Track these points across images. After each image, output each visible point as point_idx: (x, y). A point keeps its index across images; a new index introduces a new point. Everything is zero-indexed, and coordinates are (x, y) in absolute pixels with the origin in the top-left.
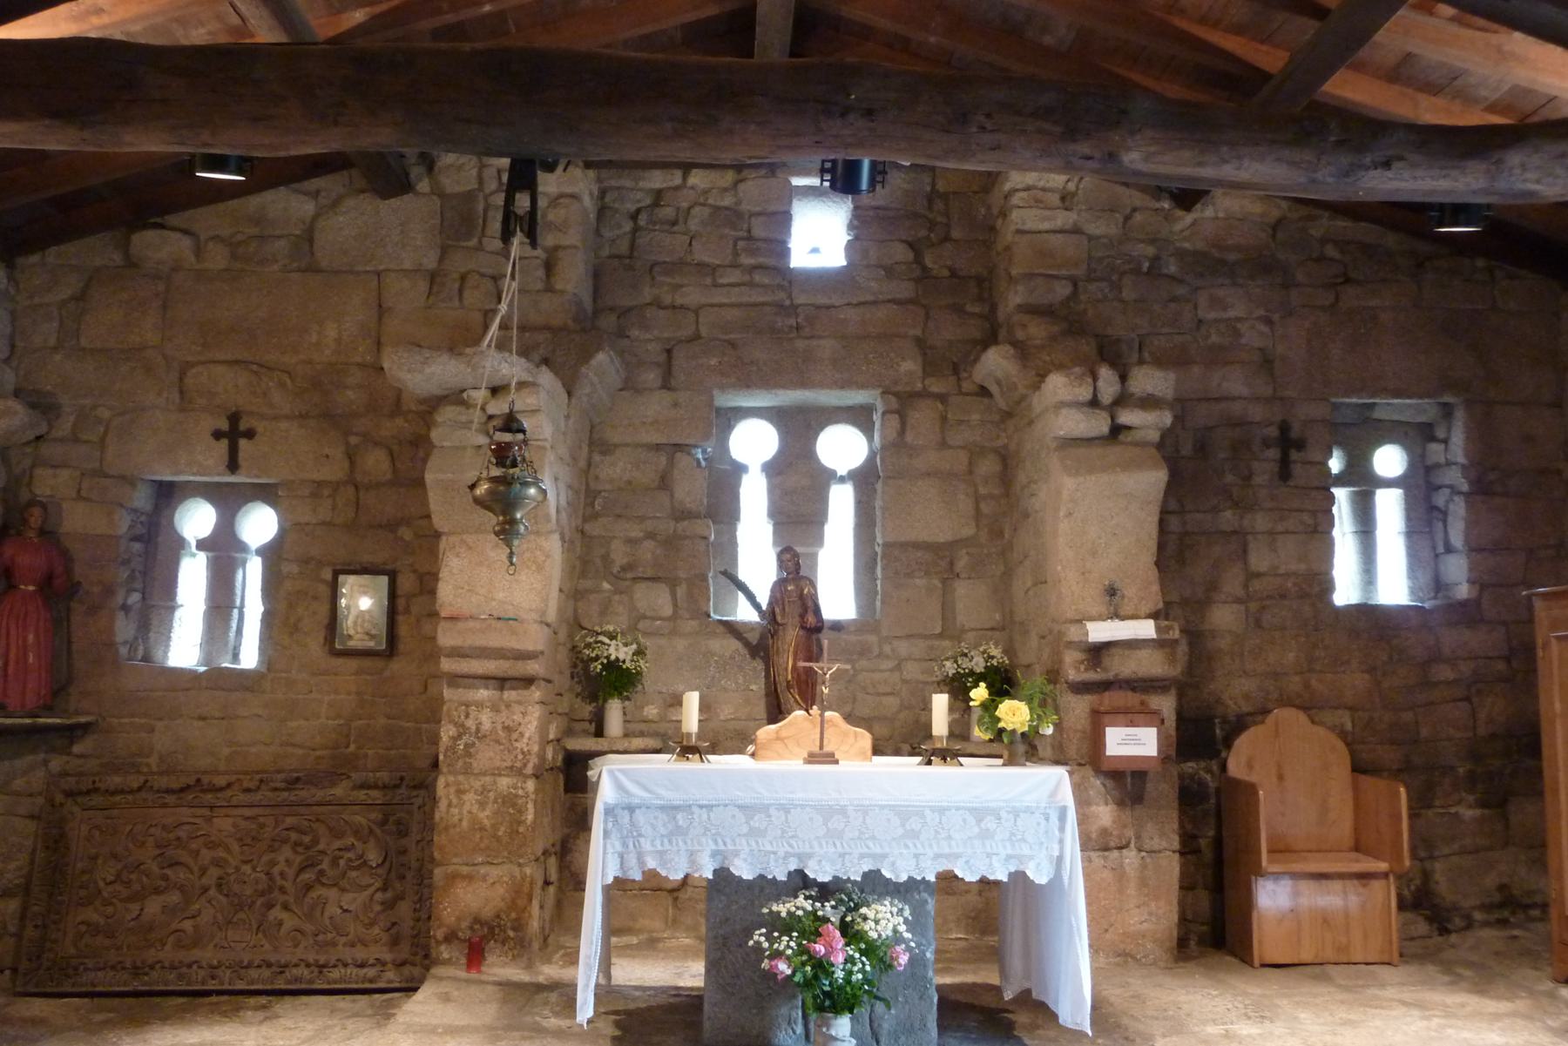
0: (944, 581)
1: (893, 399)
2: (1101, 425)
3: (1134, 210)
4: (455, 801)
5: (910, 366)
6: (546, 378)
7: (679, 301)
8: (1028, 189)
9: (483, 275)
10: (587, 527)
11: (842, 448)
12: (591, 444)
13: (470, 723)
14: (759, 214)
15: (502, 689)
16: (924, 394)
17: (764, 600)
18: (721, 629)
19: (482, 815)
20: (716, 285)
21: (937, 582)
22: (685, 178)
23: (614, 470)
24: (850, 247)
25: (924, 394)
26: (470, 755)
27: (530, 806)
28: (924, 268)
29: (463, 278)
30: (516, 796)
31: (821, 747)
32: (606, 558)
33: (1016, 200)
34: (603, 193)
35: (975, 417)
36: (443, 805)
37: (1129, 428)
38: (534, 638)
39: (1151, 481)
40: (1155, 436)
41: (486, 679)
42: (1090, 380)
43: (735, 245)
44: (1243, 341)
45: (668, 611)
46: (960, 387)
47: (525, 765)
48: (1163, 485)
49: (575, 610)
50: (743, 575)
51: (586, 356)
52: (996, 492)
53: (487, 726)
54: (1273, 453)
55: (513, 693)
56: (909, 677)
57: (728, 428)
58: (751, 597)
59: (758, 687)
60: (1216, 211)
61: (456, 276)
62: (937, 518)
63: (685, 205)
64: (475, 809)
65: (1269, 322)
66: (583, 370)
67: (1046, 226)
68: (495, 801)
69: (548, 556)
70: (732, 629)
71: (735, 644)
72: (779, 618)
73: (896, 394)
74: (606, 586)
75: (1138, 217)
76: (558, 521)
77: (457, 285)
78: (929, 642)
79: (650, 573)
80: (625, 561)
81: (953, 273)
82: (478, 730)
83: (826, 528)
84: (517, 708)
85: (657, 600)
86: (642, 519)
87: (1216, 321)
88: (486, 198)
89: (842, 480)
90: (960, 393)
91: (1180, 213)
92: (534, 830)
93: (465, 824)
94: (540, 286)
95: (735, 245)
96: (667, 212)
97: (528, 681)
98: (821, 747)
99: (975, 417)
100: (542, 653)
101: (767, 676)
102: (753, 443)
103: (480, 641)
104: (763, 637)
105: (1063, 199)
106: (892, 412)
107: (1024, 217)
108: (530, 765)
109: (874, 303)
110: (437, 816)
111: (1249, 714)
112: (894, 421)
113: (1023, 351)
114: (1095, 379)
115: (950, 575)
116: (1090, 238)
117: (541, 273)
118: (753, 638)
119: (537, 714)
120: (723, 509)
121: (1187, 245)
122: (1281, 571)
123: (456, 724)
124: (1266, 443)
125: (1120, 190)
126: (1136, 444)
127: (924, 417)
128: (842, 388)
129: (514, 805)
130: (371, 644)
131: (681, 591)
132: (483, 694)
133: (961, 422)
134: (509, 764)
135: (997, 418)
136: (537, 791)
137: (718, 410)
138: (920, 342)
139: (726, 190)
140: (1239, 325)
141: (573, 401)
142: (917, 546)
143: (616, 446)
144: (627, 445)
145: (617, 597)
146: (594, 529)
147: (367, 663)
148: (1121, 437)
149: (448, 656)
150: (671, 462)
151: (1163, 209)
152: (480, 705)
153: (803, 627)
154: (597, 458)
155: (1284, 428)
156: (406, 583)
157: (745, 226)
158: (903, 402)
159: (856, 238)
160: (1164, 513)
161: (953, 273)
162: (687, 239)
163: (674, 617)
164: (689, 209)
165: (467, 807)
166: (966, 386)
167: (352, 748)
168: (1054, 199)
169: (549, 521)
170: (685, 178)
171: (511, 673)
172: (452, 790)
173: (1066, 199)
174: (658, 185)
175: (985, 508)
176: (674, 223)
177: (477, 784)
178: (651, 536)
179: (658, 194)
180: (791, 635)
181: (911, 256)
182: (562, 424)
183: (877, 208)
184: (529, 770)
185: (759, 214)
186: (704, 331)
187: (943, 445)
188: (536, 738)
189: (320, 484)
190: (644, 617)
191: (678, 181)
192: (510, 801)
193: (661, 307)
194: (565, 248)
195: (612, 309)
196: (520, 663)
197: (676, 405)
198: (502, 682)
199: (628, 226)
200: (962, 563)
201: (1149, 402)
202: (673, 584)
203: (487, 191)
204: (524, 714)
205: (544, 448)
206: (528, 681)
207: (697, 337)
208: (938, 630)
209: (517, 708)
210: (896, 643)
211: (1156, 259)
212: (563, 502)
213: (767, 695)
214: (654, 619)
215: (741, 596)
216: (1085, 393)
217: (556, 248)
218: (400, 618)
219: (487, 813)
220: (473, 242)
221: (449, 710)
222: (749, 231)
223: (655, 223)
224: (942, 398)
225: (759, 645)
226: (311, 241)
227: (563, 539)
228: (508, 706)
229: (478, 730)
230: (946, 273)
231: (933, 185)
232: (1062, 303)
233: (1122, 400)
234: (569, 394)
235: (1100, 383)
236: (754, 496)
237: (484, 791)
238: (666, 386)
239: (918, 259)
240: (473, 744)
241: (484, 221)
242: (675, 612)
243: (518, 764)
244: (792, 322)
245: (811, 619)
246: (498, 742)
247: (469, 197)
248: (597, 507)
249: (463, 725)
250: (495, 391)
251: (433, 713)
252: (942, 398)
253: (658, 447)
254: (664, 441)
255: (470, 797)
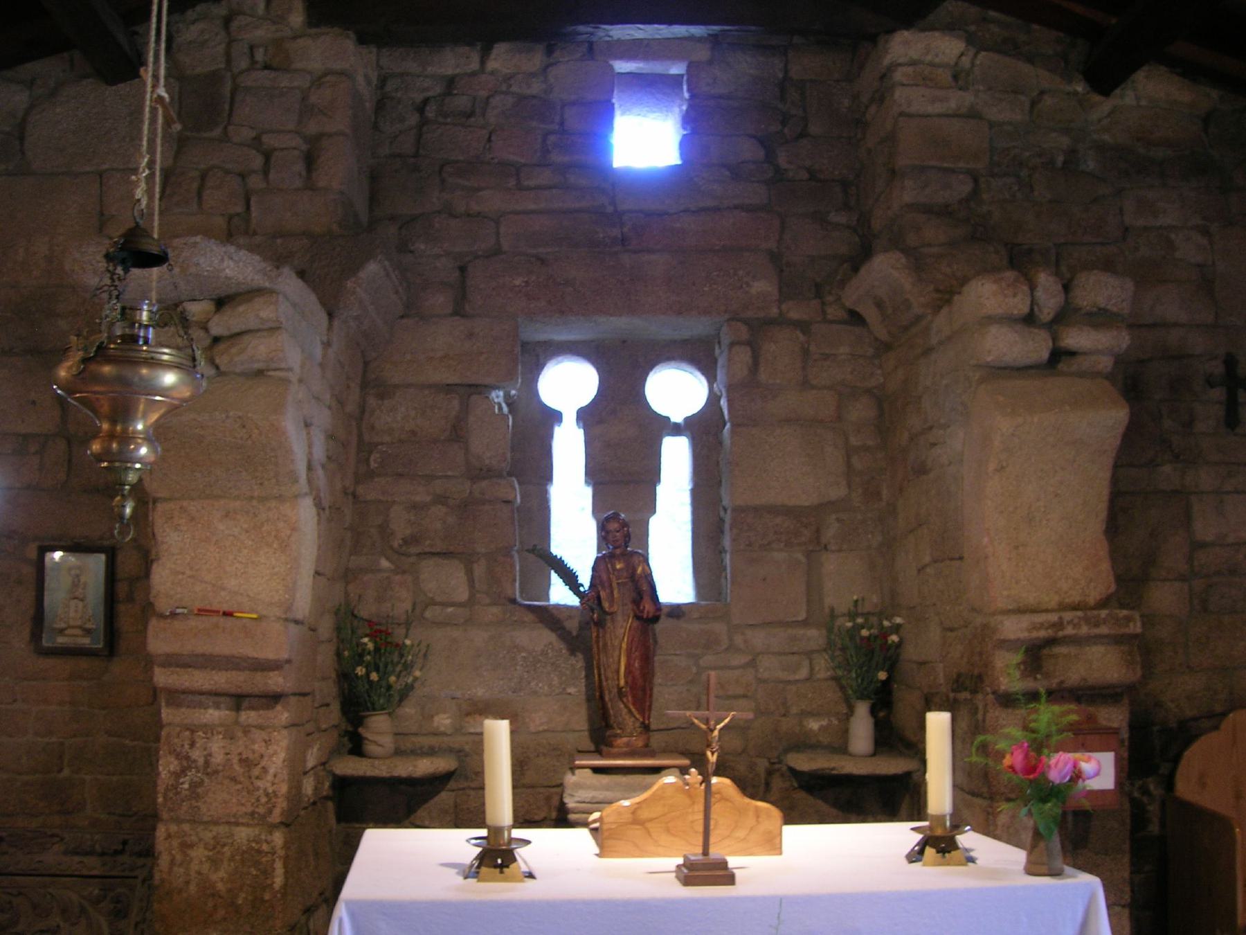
0: (808, 555)
1: (744, 329)
2: (1036, 347)
3: (1042, 93)
4: (179, 857)
5: (763, 286)
6: (289, 283)
7: (475, 208)
8: (913, 63)
9: (227, 172)
10: (360, 490)
11: (676, 391)
12: (364, 385)
13: (196, 754)
14: (573, 104)
15: (238, 708)
16: (781, 321)
17: (585, 579)
18: (529, 617)
19: (214, 877)
20: (520, 187)
21: (800, 557)
22: (483, 62)
23: (395, 417)
24: (684, 144)
25: (781, 321)
26: (197, 797)
27: (279, 865)
28: (777, 169)
29: (203, 177)
30: (259, 851)
31: (706, 852)
32: (385, 531)
33: (898, 76)
34: (383, 81)
35: (844, 350)
36: (164, 861)
37: (1072, 354)
38: (277, 643)
39: (1108, 420)
40: (1106, 363)
41: (216, 695)
42: (1026, 288)
43: (544, 140)
44: (1178, 255)
45: (463, 594)
46: (824, 312)
47: (270, 812)
48: (1121, 430)
49: (347, 594)
50: (556, 549)
51: (352, 268)
52: (870, 443)
53: (218, 759)
54: (1218, 394)
55: (253, 713)
56: (766, 675)
57: (538, 367)
58: (570, 579)
59: (577, 690)
60: (1138, 98)
61: (196, 174)
62: (797, 475)
63: (483, 94)
64: (206, 868)
65: (1205, 232)
66: (349, 284)
67: (938, 108)
68: (232, 859)
69: (294, 529)
70: (551, 617)
71: (547, 637)
72: (606, 605)
73: (746, 322)
74: (385, 563)
75: (1048, 101)
76: (309, 481)
77: (195, 185)
78: (790, 631)
79: (440, 546)
80: (408, 532)
81: (813, 175)
82: (207, 763)
83: (660, 489)
84: (258, 735)
85: (447, 580)
86: (430, 478)
87: (1146, 229)
88: (234, 78)
89: (676, 430)
90: (825, 321)
91: (1097, 98)
92: (284, 895)
93: (193, 888)
94: (298, 183)
95: (544, 140)
96: (461, 102)
97: (274, 699)
98: (706, 852)
99: (844, 350)
100: (289, 661)
101: (589, 685)
102: (568, 384)
103: (203, 646)
104: (584, 626)
105: (955, 77)
106: (739, 343)
107: (910, 97)
108: (277, 811)
109: (717, 210)
110: (157, 876)
111: (1195, 719)
112: (744, 355)
113: (918, 263)
114: (1033, 288)
115: (816, 546)
116: (992, 125)
117: (300, 167)
118: (572, 625)
119: (284, 743)
120: (536, 469)
121: (1106, 137)
122: (1230, 540)
123: (178, 756)
124: (1210, 383)
125: (1025, 68)
126: (1081, 375)
127: (781, 350)
128: (680, 313)
129: (257, 864)
130: (86, 641)
131: (479, 570)
132: (213, 715)
133: (826, 357)
134: (250, 809)
135: (870, 351)
136: (286, 846)
137: (525, 345)
138: (775, 258)
139: (533, 75)
140: (1173, 236)
141: (336, 323)
142: (773, 510)
143: (396, 386)
144: (409, 386)
145: (397, 578)
146: (370, 492)
147: (84, 663)
148: (1062, 366)
149: (163, 665)
150: (465, 408)
151: (1076, 93)
152: (209, 729)
153: (637, 617)
154: (372, 401)
155: (1230, 363)
156: (128, 563)
157: (557, 119)
158: (757, 330)
159: (694, 132)
160: (1116, 466)
161: (813, 175)
162: (485, 133)
163: (471, 602)
164: (488, 98)
165: (194, 867)
166: (833, 312)
167: (66, 772)
168: (945, 76)
169: (296, 481)
170: (483, 62)
171: (247, 689)
172: (175, 843)
173: (959, 77)
174: (450, 72)
175: (856, 462)
176: (470, 115)
177: (208, 836)
178: (441, 499)
179: (451, 82)
180: (621, 630)
181: (761, 154)
182: (318, 351)
183: (720, 97)
184: (276, 817)
185: (573, 104)
186: (505, 246)
187: (806, 384)
188: (284, 774)
189: (26, 437)
190: (433, 603)
191: (475, 65)
192: (252, 856)
193: (452, 215)
194: (330, 135)
195: (392, 218)
196: (259, 676)
197: (471, 335)
198: (239, 700)
199: (413, 119)
200: (831, 531)
201: (1100, 318)
202: (468, 560)
203: (235, 71)
204: (267, 742)
205: (286, 381)
206: (274, 699)
207: (497, 251)
208: (802, 616)
209: (258, 735)
210: (749, 633)
211: (1072, 153)
212: (319, 453)
213: (589, 700)
214: (445, 605)
215: (554, 577)
216: (1020, 305)
217: (320, 136)
218: (121, 608)
219: (222, 874)
220: (217, 132)
221: (168, 735)
222: (562, 124)
223: (446, 116)
224: (803, 326)
225: (581, 633)
226: (22, 139)
227: (318, 505)
228: (246, 730)
229: (207, 763)
230: (804, 175)
231: (786, 71)
232: (960, 202)
233: (1063, 317)
234: (330, 315)
235: (1039, 293)
236: (569, 449)
237: (217, 844)
238: (459, 311)
239: (770, 156)
240: (201, 783)
241: (231, 110)
242: (472, 596)
243: (261, 810)
244: (616, 232)
245: (648, 607)
246: (234, 780)
247: (214, 78)
248: (373, 465)
249: (188, 758)
250: (221, 303)
251: (149, 737)
252: (803, 326)
253: (449, 388)
254: (458, 381)
255: (199, 853)
